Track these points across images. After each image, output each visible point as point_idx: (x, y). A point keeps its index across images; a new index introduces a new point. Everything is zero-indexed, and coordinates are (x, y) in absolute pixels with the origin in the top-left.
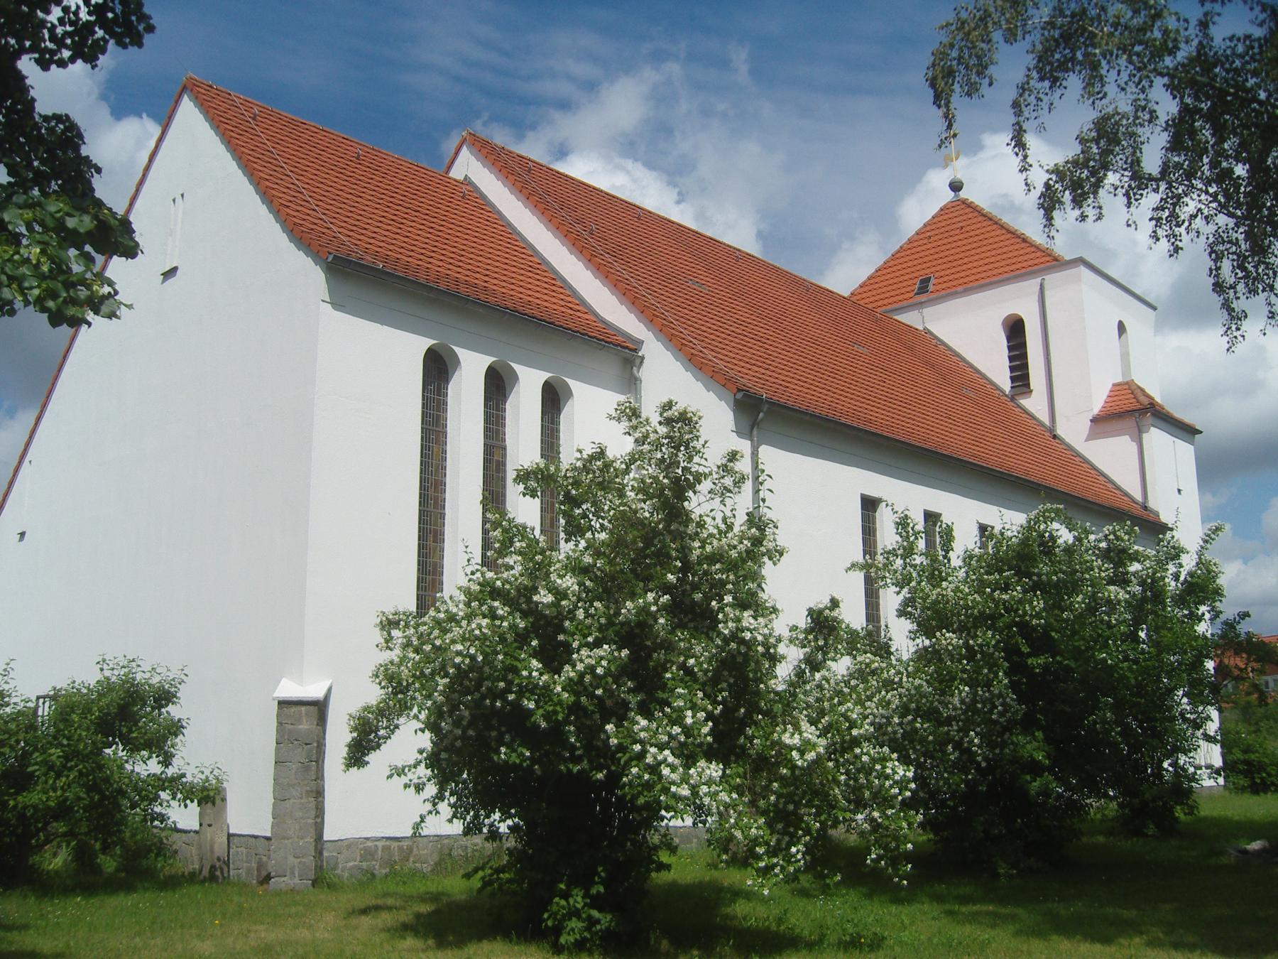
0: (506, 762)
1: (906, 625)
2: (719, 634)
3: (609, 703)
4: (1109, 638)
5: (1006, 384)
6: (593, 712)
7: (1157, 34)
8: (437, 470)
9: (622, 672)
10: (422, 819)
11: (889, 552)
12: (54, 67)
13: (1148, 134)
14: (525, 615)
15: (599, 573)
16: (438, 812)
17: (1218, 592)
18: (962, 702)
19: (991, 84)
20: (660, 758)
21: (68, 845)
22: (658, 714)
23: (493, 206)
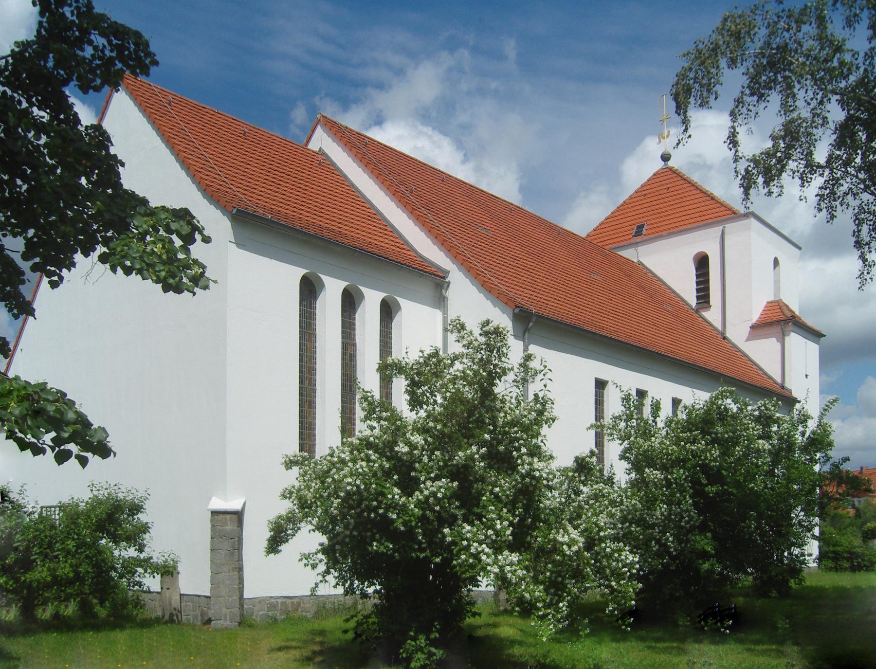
0: (376, 552)
1: (625, 465)
2: (518, 472)
3: (444, 515)
4: (756, 474)
5: (693, 301)
6: (433, 521)
7: (835, 63)
8: (310, 360)
9: (454, 496)
10: (317, 585)
11: (616, 418)
12: (91, 91)
13: (820, 134)
14: (389, 459)
15: (436, 433)
16: (326, 581)
17: (830, 444)
18: (662, 514)
19: (716, 99)
20: (480, 549)
21: (75, 600)
22: (477, 522)
23: (341, 171)
